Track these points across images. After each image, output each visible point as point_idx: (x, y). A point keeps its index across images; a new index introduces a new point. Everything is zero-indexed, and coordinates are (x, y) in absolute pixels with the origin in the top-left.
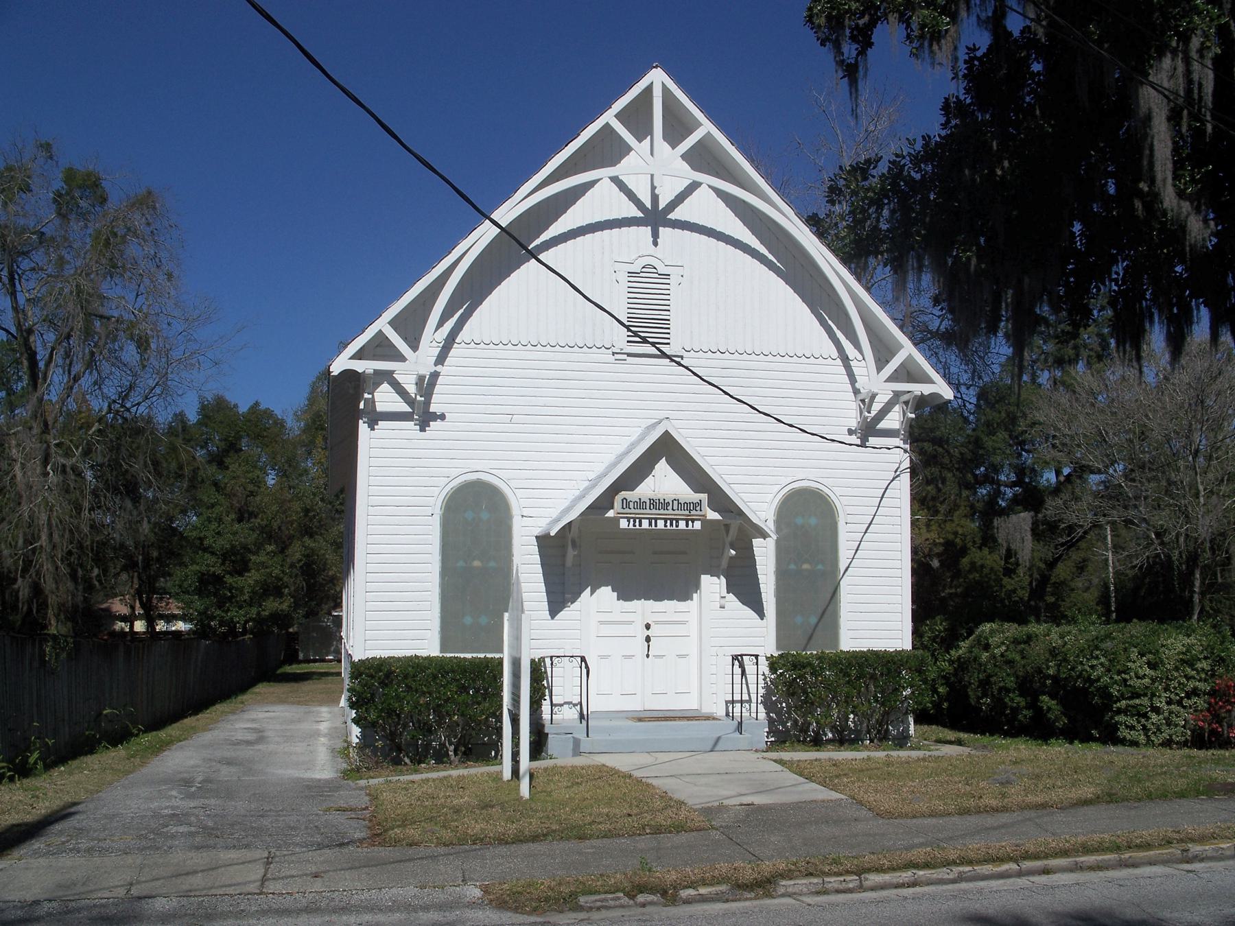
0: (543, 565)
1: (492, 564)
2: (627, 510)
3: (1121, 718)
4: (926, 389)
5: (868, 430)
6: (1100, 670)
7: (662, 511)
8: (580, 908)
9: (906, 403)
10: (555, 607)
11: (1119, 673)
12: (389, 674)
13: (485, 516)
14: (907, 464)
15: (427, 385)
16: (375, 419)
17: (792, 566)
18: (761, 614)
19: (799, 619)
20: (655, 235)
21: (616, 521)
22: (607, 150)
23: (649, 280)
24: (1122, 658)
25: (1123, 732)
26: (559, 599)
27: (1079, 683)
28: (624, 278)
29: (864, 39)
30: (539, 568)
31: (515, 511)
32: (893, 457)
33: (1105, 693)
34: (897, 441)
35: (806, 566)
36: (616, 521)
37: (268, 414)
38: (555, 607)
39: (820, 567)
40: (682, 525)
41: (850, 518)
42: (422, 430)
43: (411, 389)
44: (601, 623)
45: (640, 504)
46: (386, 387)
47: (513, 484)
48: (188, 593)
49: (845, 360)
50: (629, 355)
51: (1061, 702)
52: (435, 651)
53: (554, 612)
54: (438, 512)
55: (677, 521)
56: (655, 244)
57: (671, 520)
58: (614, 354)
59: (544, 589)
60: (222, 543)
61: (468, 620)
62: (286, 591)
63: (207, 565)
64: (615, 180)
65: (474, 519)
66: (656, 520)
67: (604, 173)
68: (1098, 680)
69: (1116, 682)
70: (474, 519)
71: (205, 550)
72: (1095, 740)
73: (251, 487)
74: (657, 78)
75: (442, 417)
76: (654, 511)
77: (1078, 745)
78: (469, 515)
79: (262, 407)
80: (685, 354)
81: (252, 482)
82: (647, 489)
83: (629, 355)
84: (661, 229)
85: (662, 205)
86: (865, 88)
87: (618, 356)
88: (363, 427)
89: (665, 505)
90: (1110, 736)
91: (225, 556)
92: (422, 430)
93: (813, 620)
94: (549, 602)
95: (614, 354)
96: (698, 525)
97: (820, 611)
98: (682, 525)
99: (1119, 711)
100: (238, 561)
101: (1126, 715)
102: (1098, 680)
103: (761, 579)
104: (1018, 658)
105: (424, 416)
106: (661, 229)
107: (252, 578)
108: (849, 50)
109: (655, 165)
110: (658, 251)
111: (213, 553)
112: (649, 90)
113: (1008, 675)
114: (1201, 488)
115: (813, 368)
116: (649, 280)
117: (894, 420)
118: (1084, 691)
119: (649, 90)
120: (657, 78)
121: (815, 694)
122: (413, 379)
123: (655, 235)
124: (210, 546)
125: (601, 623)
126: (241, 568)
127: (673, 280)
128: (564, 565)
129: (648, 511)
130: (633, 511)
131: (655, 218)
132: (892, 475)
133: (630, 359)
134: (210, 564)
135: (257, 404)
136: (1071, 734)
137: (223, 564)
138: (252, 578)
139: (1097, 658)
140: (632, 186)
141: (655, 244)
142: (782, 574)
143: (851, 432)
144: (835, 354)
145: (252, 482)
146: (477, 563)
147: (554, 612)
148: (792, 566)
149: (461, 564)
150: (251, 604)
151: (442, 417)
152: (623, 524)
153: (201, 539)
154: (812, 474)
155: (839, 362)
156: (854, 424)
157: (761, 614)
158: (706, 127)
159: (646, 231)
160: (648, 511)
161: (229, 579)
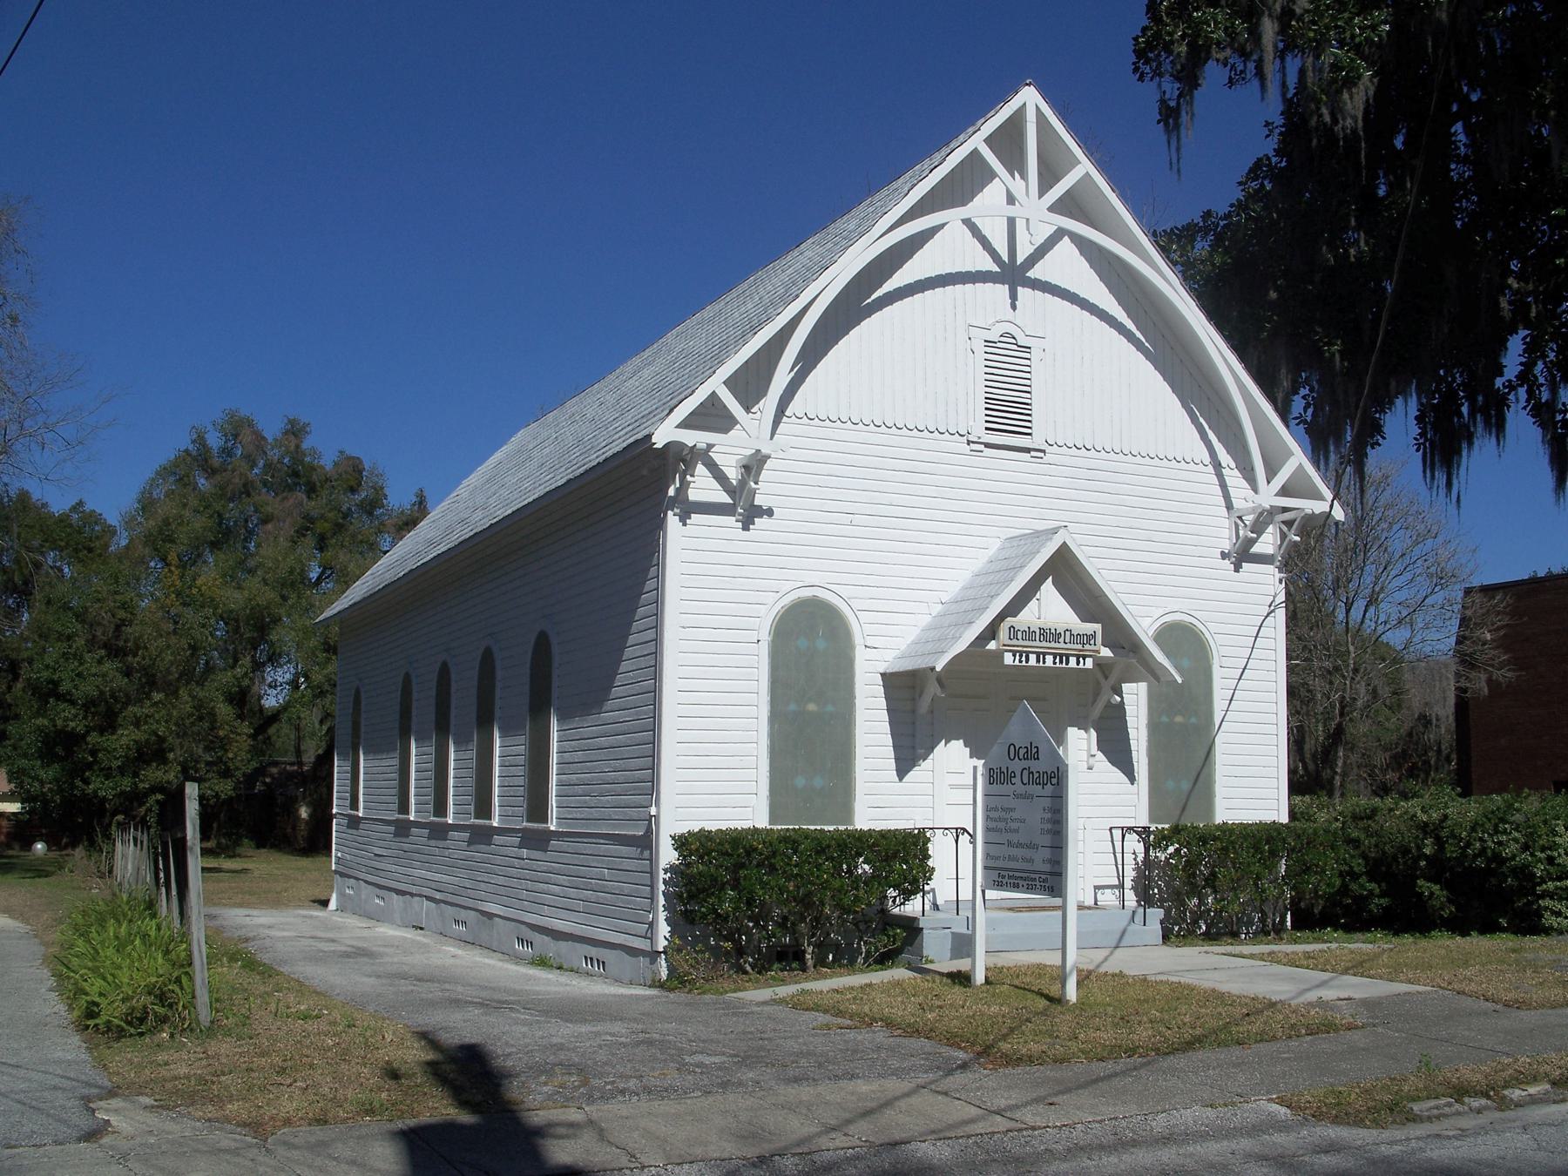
0: (890, 710)
1: (830, 708)
2: (1015, 642)
3: (1546, 902)
4: (1319, 507)
5: (1242, 555)
6: (1514, 847)
7: (1053, 645)
8: (1414, 1119)
9: (1289, 524)
10: (904, 764)
11: (1543, 849)
12: (750, 851)
13: (821, 644)
14: (1282, 597)
15: (753, 466)
16: (688, 510)
17: (1165, 719)
18: (1132, 780)
19: (1170, 784)
20: (1014, 297)
21: (998, 655)
22: (962, 186)
23: (1007, 352)
24: (1543, 830)
25: (1549, 920)
26: (908, 755)
27: (1480, 863)
28: (980, 347)
29: (1189, 78)
30: (885, 715)
31: (858, 640)
32: (1267, 583)
33: (1524, 873)
34: (1270, 569)
35: (1179, 719)
36: (998, 655)
37: (93, 518)
38: (904, 764)
39: (1193, 720)
40: (1073, 662)
41: (1226, 662)
42: (746, 528)
43: (733, 474)
44: (953, 787)
45: (1029, 634)
46: (700, 469)
47: (856, 604)
48: (25, 756)
49: (1218, 466)
50: (987, 445)
51: (1447, 885)
52: (762, 822)
53: (902, 772)
54: (766, 637)
55: (1068, 657)
56: (1014, 307)
57: (1061, 656)
58: (969, 442)
59: (890, 741)
60: (88, 689)
61: (800, 782)
62: (171, 756)
63: (66, 719)
64: (968, 222)
65: (809, 645)
66: (1044, 654)
67: (952, 217)
68: (1514, 857)
69: (1540, 861)
70: (809, 645)
71: (61, 697)
72: (1503, 930)
73: (122, 614)
74: (1029, 98)
75: (770, 512)
76: (1044, 644)
77: (1407, 939)
78: (802, 643)
79: (88, 507)
80: (1048, 449)
81: (124, 606)
82: (1028, 617)
83: (987, 445)
84: (1019, 289)
85: (1020, 260)
86: (1189, 135)
87: (974, 446)
88: (672, 520)
89: (1056, 636)
90: (1529, 924)
91: (89, 705)
92: (746, 528)
93: (1186, 785)
94: (897, 759)
95: (969, 442)
96: (1089, 663)
97: (1194, 774)
98: (1073, 662)
99: (1542, 896)
100: (107, 715)
101: (1552, 898)
102: (1514, 857)
103: (1132, 733)
104: (1363, 837)
105: (745, 507)
106: (1019, 289)
107: (125, 738)
108: (1171, 88)
109: (1013, 207)
110: (1018, 317)
111: (73, 703)
112: (1021, 111)
113: (1352, 857)
114: (1352, 648)
115: (1074, 461)
116: (1007, 352)
117: (1267, 543)
118: (1488, 872)
119: (1021, 111)
120: (1029, 98)
121: (1200, 876)
122: (733, 460)
123: (1014, 297)
124: (69, 693)
125: (953, 787)
126: (109, 724)
127: (1035, 354)
128: (914, 712)
129: (1037, 643)
130: (1021, 642)
131: (1013, 275)
132: (1266, 610)
133: (988, 451)
134: (68, 717)
135: (80, 503)
136: (1459, 926)
137: (85, 718)
138: (125, 738)
139: (1505, 832)
140: (986, 232)
141: (1014, 307)
142: (1154, 727)
143: (1224, 556)
144: (1207, 460)
145: (124, 606)
146: (812, 707)
147: (902, 772)
148: (1165, 719)
149: (793, 707)
150: (122, 771)
151: (770, 512)
152: (1008, 659)
153: (56, 684)
154: (1184, 605)
155: (1211, 469)
156: (1227, 546)
157: (1132, 780)
158: (1084, 167)
159: (1003, 290)
160: (1037, 643)
161: (93, 738)
